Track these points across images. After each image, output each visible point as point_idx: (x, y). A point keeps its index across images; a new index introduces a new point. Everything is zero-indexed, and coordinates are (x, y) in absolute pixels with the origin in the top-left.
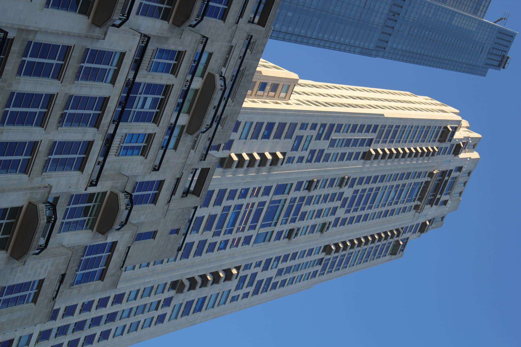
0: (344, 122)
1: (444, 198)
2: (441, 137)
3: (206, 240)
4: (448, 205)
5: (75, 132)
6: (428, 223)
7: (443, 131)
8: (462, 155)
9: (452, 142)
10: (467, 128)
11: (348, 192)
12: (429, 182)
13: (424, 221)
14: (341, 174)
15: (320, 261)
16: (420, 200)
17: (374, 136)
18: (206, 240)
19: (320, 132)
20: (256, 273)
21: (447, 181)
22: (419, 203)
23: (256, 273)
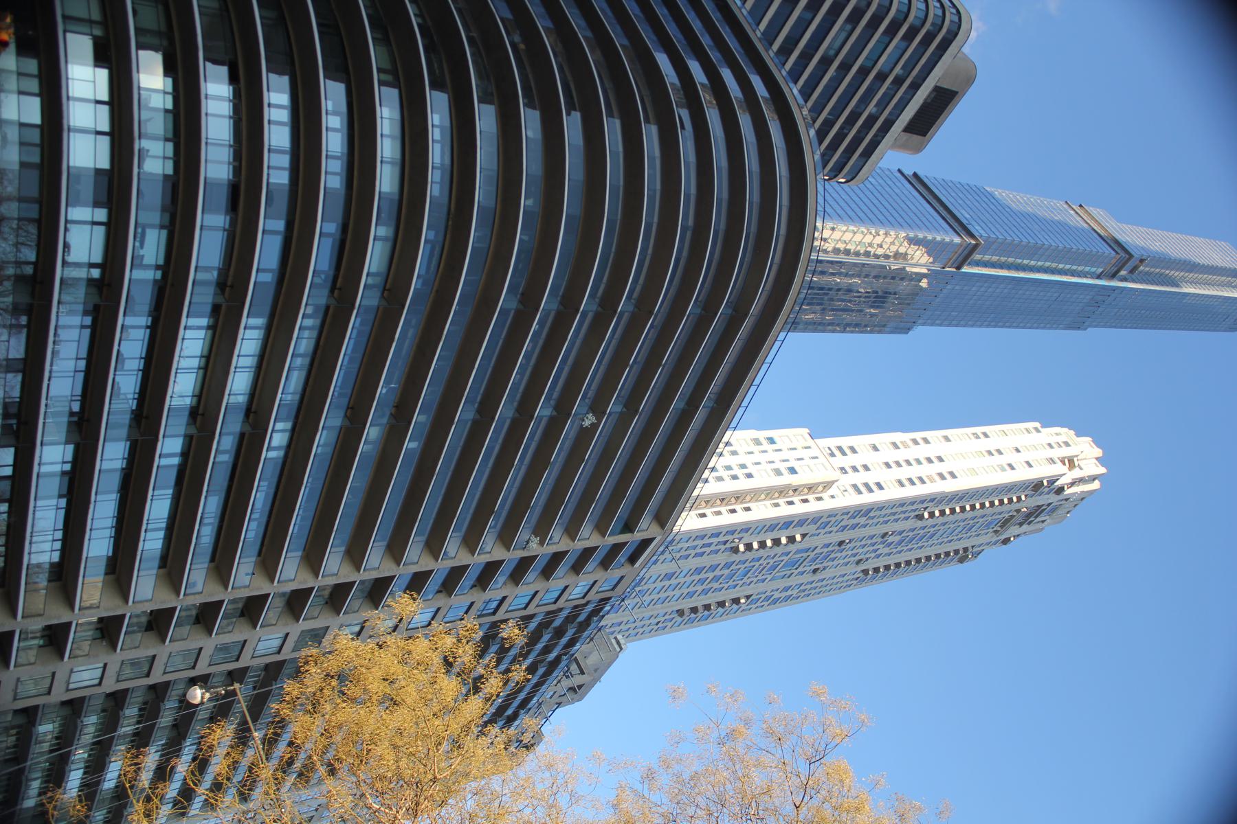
1: (1039, 519)
10: (1097, 459)
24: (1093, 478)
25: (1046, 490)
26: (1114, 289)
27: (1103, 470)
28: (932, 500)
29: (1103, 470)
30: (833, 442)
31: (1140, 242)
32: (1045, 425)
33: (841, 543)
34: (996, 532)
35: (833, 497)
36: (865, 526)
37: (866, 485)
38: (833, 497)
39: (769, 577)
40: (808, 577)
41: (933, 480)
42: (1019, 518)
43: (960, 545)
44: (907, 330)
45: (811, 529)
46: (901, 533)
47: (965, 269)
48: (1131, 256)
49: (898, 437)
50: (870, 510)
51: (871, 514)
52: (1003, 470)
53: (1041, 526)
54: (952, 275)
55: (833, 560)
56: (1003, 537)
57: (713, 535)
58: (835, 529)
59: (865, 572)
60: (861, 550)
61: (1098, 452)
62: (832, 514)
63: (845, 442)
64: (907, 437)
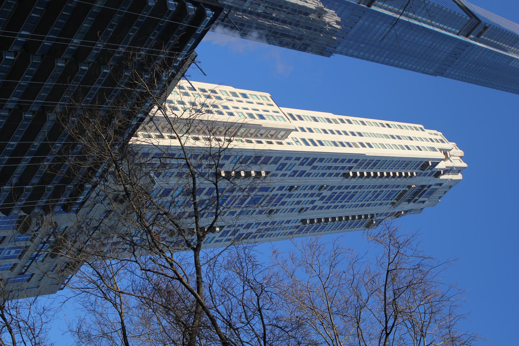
0: (326, 157)
1: (421, 199)
2: (421, 167)
3: (306, 171)
4: (425, 204)
5: (466, 25)
6: (403, 212)
7: (424, 164)
8: (442, 177)
9: (433, 170)
10: (461, 157)
11: (326, 193)
12: (407, 191)
13: (400, 211)
14: (321, 184)
15: (297, 227)
16: (397, 200)
17: (355, 165)
18: (306, 171)
19: (304, 162)
20: (315, 201)
21: (426, 190)
22: (395, 201)
23: (315, 201)
24: (459, 170)
25: (429, 171)
26: (468, 44)
27: (464, 165)
28: (356, 161)
29: (464, 165)
30: (287, 110)
31: (483, 15)
32: (427, 127)
33: (291, 188)
34: (393, 204)
35: (289, 144)
36: (308, 175)
37: (312, 140)
38: (289, 144)
39: (239, 210)
40: (263, 218)
41: (357, 146)
42: (407, 196)
43: (369, 211)
44: (329, 54)
45: (273, 168)
46: (332, 188)
47: (373, 8)
48: (480, 21)
49: (330, 116)
50: (314, 160)
51: (315, 164)
52: (403, 148)
53: (421, 206)
54: (364, 11)
55: (283, 204)
56: (397, 210)
57: (205, 157)
58: (289, 173)
59: (304, 221)
60: (303, 199)
61: (461, 153)
62: (289, 156)
63: (295, 112)
64: (337, 117)
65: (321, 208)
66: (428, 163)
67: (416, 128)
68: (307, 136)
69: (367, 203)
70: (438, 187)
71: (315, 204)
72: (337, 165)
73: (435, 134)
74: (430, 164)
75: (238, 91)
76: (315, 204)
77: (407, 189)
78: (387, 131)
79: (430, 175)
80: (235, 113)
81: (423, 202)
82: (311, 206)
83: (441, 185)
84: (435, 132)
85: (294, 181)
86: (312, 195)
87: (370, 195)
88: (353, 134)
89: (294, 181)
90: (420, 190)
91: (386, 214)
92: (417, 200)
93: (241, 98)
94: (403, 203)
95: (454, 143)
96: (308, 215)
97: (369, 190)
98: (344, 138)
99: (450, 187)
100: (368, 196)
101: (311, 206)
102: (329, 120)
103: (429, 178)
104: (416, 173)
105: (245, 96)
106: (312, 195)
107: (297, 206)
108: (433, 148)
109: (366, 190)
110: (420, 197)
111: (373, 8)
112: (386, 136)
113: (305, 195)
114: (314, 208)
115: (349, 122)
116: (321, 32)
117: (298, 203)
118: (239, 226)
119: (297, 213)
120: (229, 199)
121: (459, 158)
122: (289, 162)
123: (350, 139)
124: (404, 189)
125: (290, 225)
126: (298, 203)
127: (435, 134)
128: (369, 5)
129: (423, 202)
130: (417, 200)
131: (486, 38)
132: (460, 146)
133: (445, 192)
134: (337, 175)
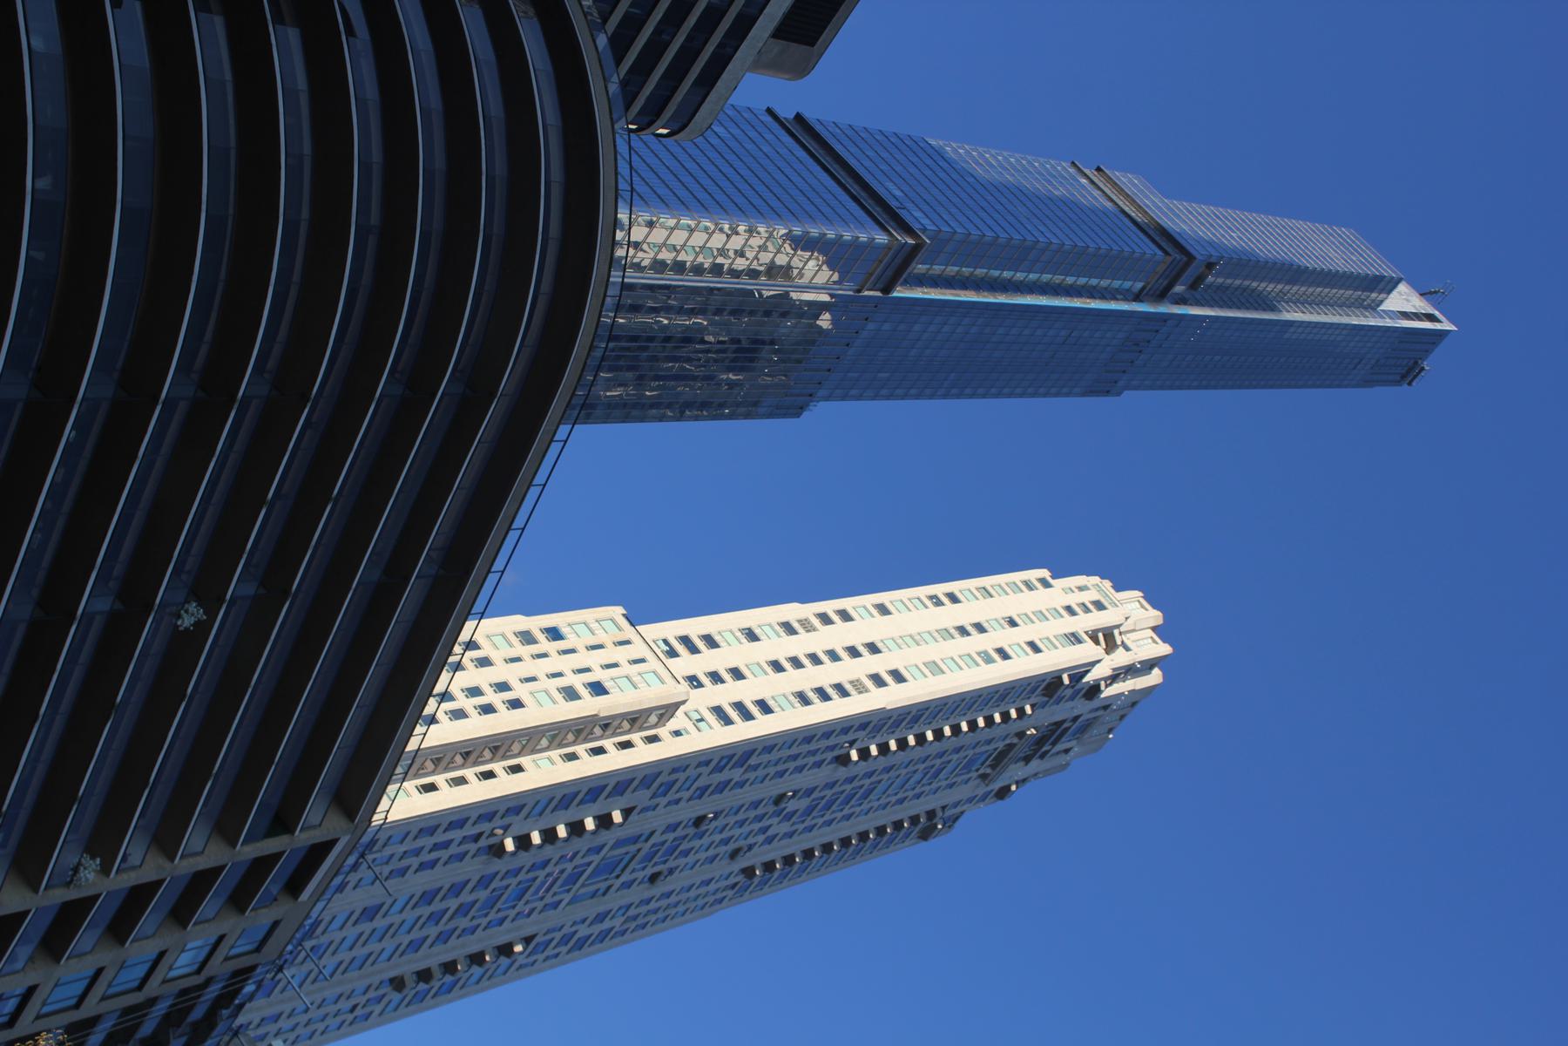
1: (1060, 747)
2: (1046, 688)
4: (1071, 753)
7: (1049, 685)
10: (1154, 629)
14: (776, 792)
16: (993, 767)
17: (861, 734)
21: (1067, 729)
22: (989, 771)
24: (1148, 666)
27: (1164, 649)
28: (863, 726)
29: (1164, 649)
31: (1205, 233)
34: (984, 777)
35: (677, 733)
36: (741, 785)
38: (677, 733)
44: (797, 410)
48: (1191, 258)
49: (792, 611)
51: (753, 761)
53: (1063, 759)
55: (686, 853)
56: (997, 786)
58: (686, 795)
59: (749, 872)
64: (809, 610)
65: (790, 835)
66: (1060, 678)
67: (1029, 585)
68: (726, 694)
69: (910, 794)
70: (1100, 713)
71: (770, 833)
72: (813, 746)
73: (1081, 589)
74: (1066, 681)
75: (536, 623)
76: (770, 833)
77: (1015, 740)
78: (951, 615)
79: (1072, 698)
80: (526, 699)
81: (1067, 751)
82: (761, 838)
83: (1106, 708)
84: (1081, 580)
85: (706, 807)
86: (760, 818)
87: (917, 777)
88: (853, 652)
89: (706, 807)
90: (1053, 732)
91: (970, 800)
92: (1046, 752)
93: (545, 645)
94: (1012, 767)
95: (1137, 594)
96: (756, 858)
97: (911, 768)
98: (827, 675)
99: (1134, 704)
100: (912, 781)
101: (761, 838)
102: (788, 628)
103: (1070, 704)
104: (1033, 706)
105: (554, 634)
106: (760, 818)
107: (723, 849)
108: (1073, 634)
109: (904, 772)
110: (1054, 744)
111: (899, 293)
112: (945, 634)
113: (741, 824)
114: (769, 840)
115: (845, 616)
116: (784, 315)
117: (726, 842)
118: (574, 923)
119: (726, 861)
120: (538, 882)
121: (1150, 633)
122: (682, 776)
123: (847, 670)
124: (1008, 741)
125: (712, 887)
126: (726, 842)
127: (1081, 589)
128: (887, 290)
129: (1067, 751)
130: (1046, 752)
131: (1220, 280)
132: (1153, 600)
133: (1122, 717)
134: (818, 765)
